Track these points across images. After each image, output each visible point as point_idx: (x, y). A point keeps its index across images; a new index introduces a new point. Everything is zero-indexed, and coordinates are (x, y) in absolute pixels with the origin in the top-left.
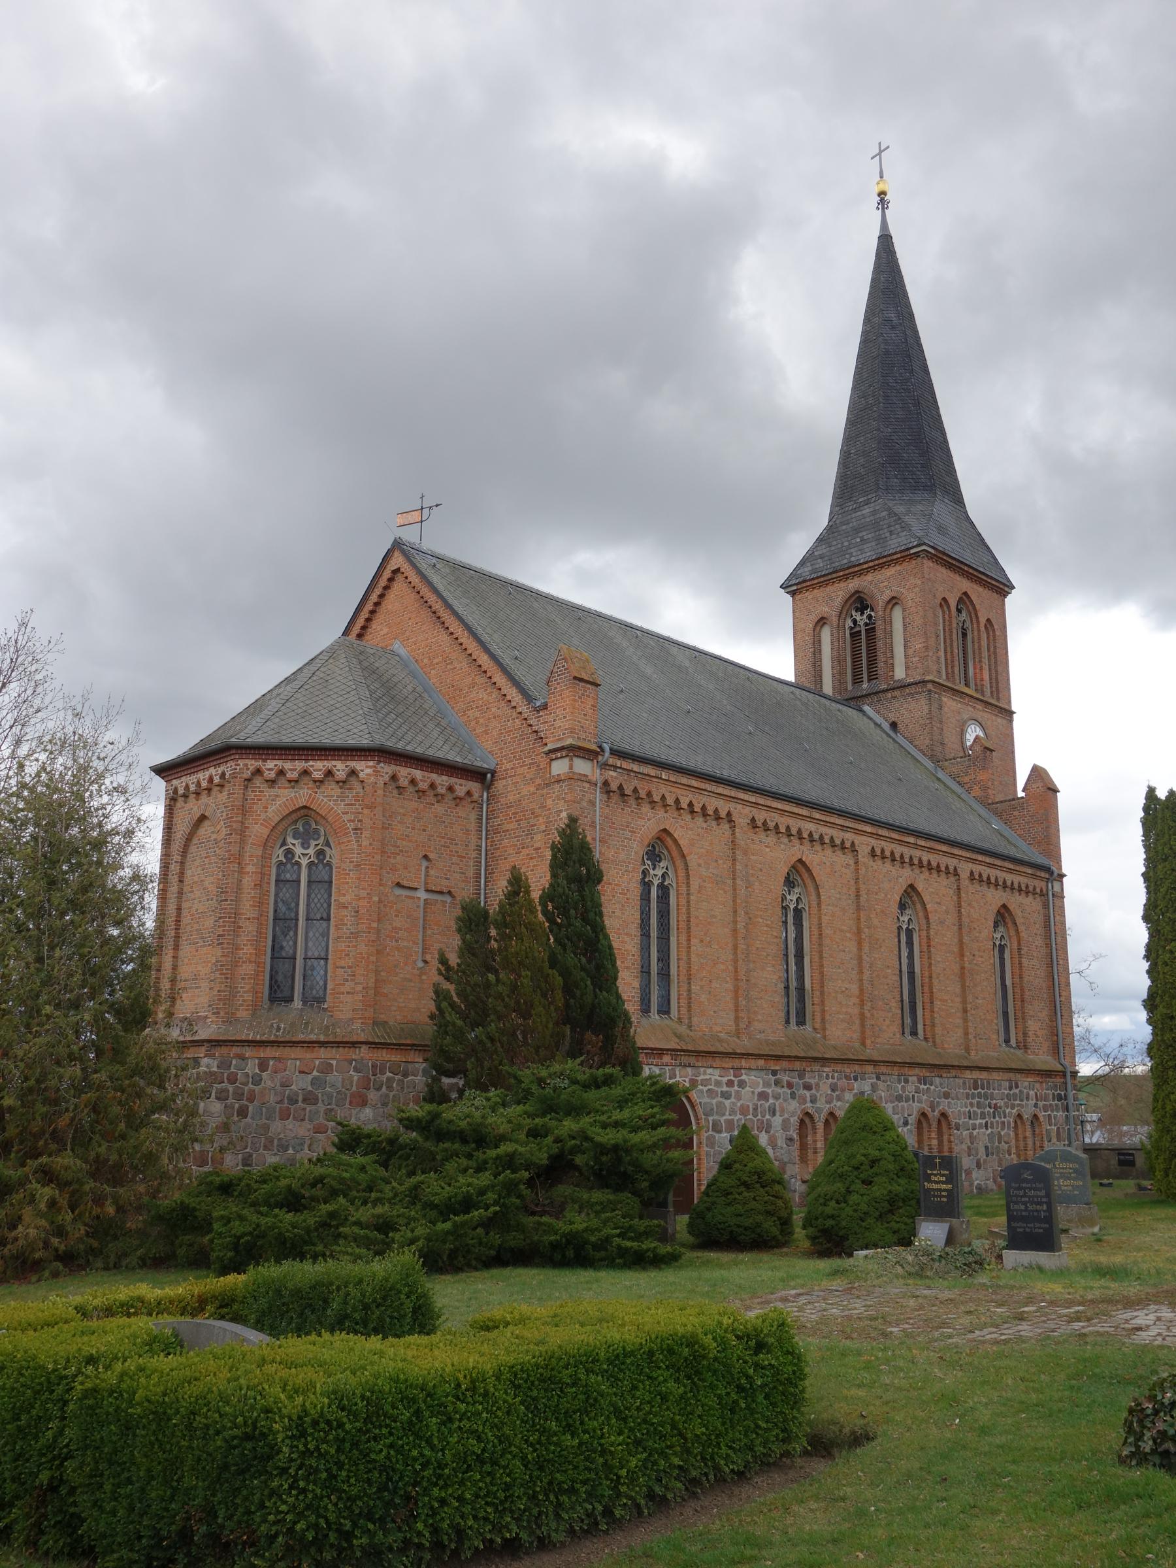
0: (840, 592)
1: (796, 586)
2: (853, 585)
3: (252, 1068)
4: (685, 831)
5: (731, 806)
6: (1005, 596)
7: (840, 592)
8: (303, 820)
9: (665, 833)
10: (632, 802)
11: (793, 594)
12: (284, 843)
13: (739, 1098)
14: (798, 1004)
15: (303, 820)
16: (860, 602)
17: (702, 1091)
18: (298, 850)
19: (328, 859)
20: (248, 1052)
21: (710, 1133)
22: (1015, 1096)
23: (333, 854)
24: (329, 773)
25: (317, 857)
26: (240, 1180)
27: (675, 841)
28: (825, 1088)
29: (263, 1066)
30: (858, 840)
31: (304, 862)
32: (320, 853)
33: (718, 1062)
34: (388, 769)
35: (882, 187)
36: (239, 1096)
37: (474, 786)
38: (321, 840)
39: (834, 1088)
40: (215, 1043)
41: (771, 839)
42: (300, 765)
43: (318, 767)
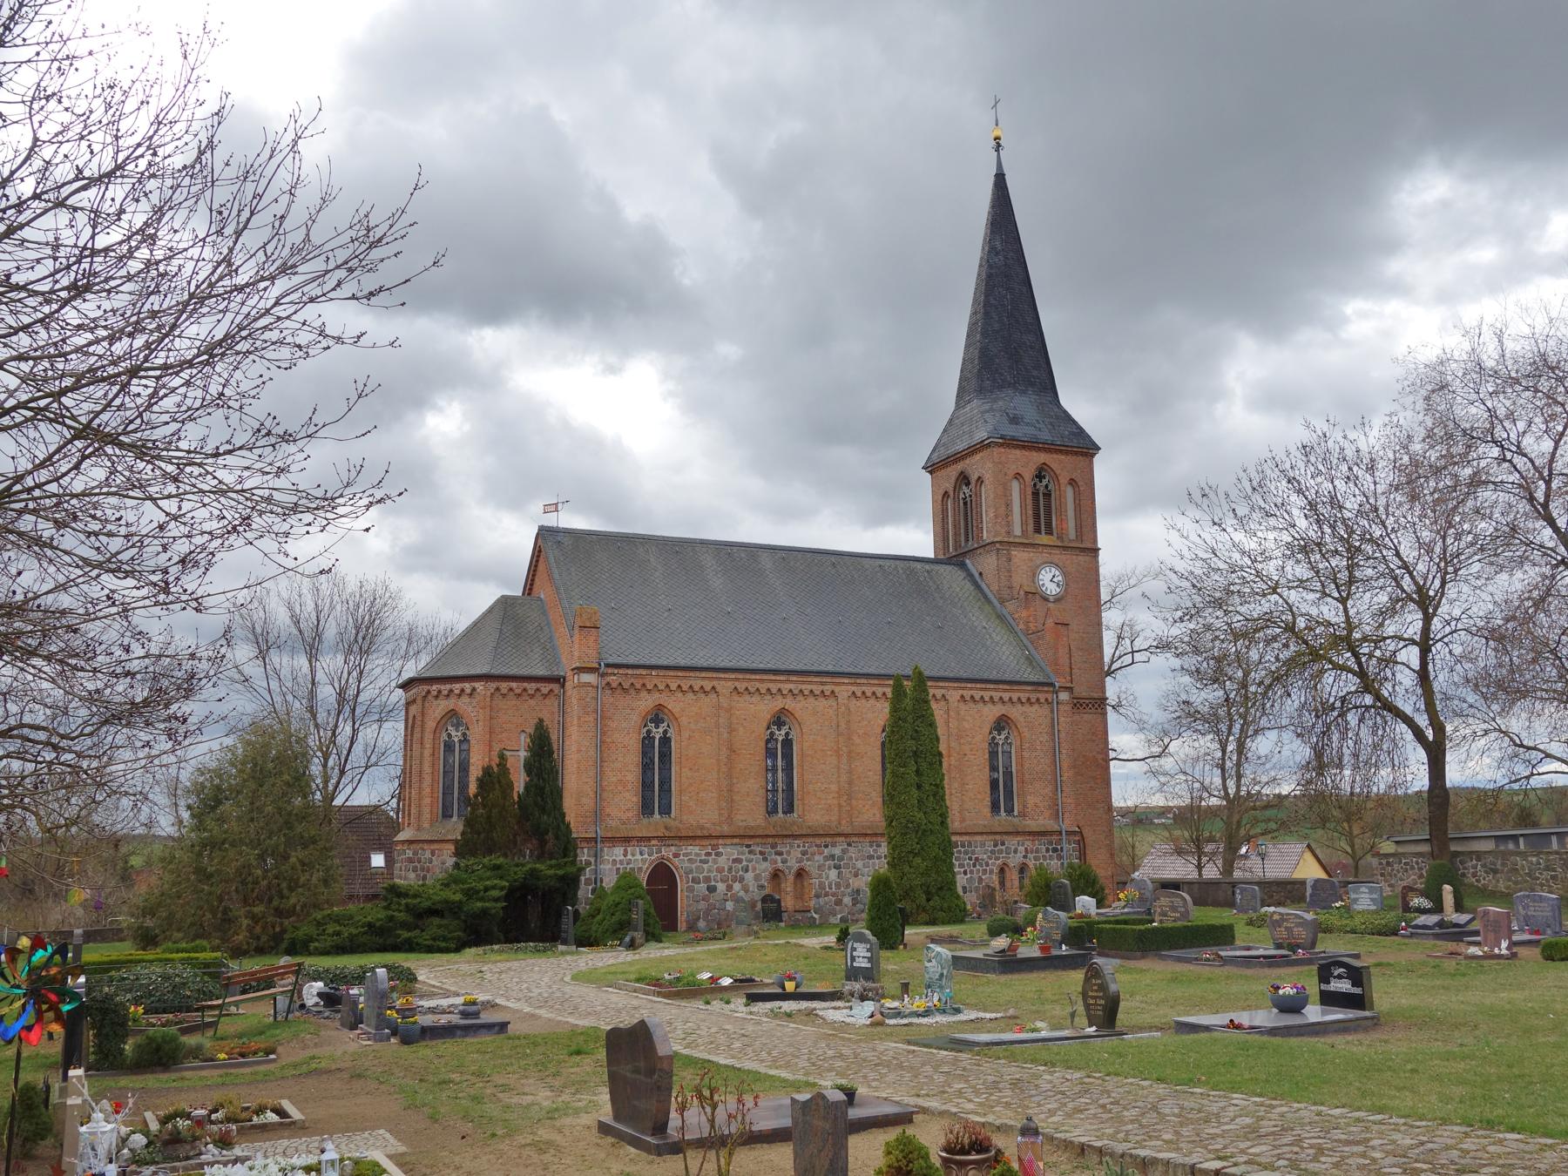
0: (953, 472)
1: (932, 468)
2: (959, 467)
3: (428, 854)
4: (674, 704)
5: (715, 683)
6: (1093, 455)
7: (953, 472)
8: (453, 716)
9: (660, 707)
10: (632, 691)
11: (931, 472)
13: (715, 862)
14: (782, 798)
15: (453, 716)
16: (964, 479)
20: (426, 846)
22: (1001, 852)
24: (451, 691)
28: (796, 853)
29: (433, 853)
30: (837, 689)
32: (464, 735)
34: (493, 685)
35: (997, 133)
36: (423, 869)
37: (555, 687)
39: (804, 853)
40: (410, 842)
41: (756, 698)
42: (448, 687)
43: (457, 687)
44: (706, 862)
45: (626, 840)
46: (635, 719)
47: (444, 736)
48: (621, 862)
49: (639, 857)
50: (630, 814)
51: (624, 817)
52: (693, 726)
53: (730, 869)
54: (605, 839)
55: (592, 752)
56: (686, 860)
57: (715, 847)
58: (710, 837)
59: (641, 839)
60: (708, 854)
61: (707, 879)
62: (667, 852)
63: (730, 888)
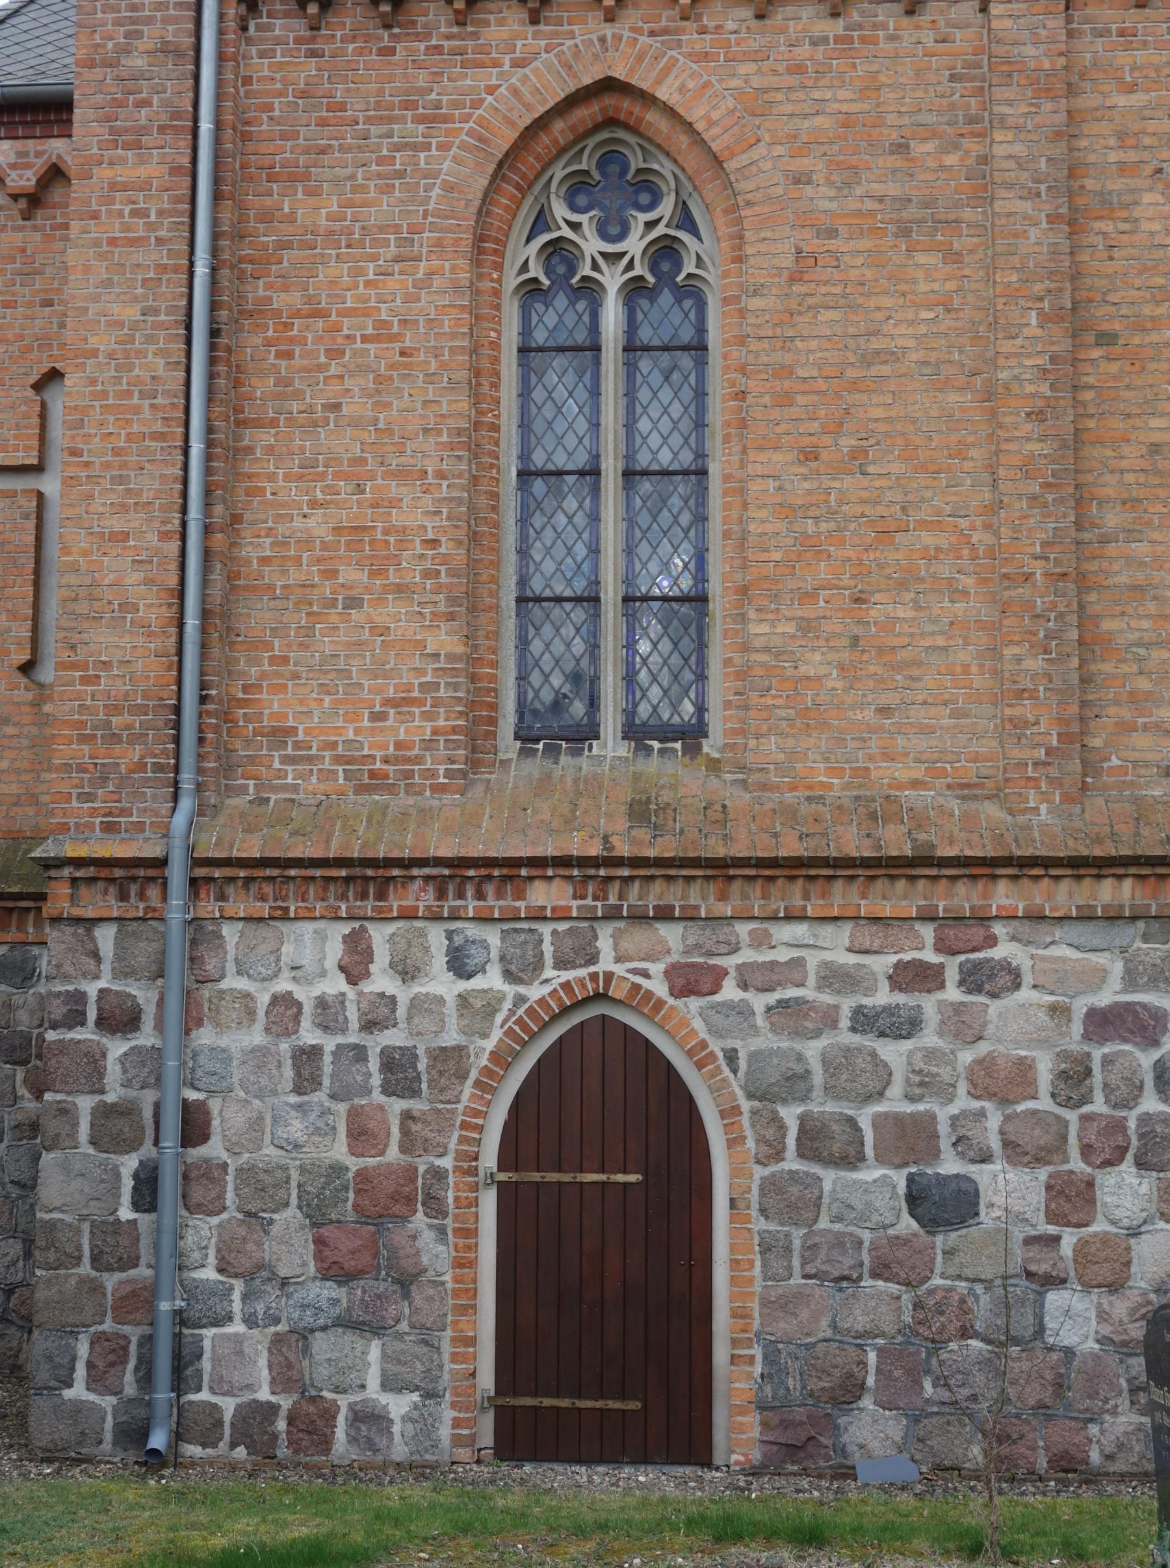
12: (541, 222)
13: (962, 1024)
17: (744, 1011)
18: (592, 245)
19: (689, 267)
21: (791, 1163)
23: (702, 252)
25: (654, 268)
26: (959, 1549)
27: (670, 112)
31: (612, 281)
32: (665, 252)
33: (841, 896)
38: (666, 208)
44: (903, 1026)
45: (364, 879)
46: (456, 170)
47: (525, 255)
48: (328, 1013)
49: (442, 984)
50: (414, 728)
51: (377, 744)
52: (822, 199)
53: (1074, 1079)
54: (210, 875)
55: (156, 362)
56: (752, 1014)
57: (963, 930)
58: (919, 865)
59: (458, 874)
60: (916, 977)
61: (910, 1139)
62: (633, 960)
63: (1071, 1200)
